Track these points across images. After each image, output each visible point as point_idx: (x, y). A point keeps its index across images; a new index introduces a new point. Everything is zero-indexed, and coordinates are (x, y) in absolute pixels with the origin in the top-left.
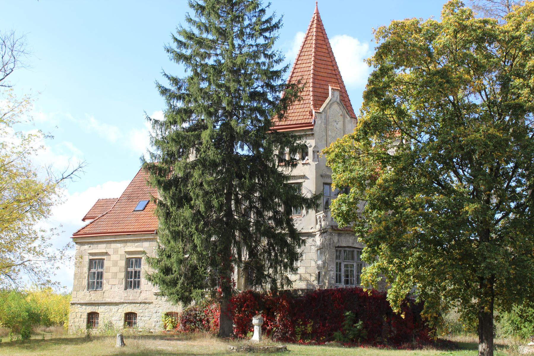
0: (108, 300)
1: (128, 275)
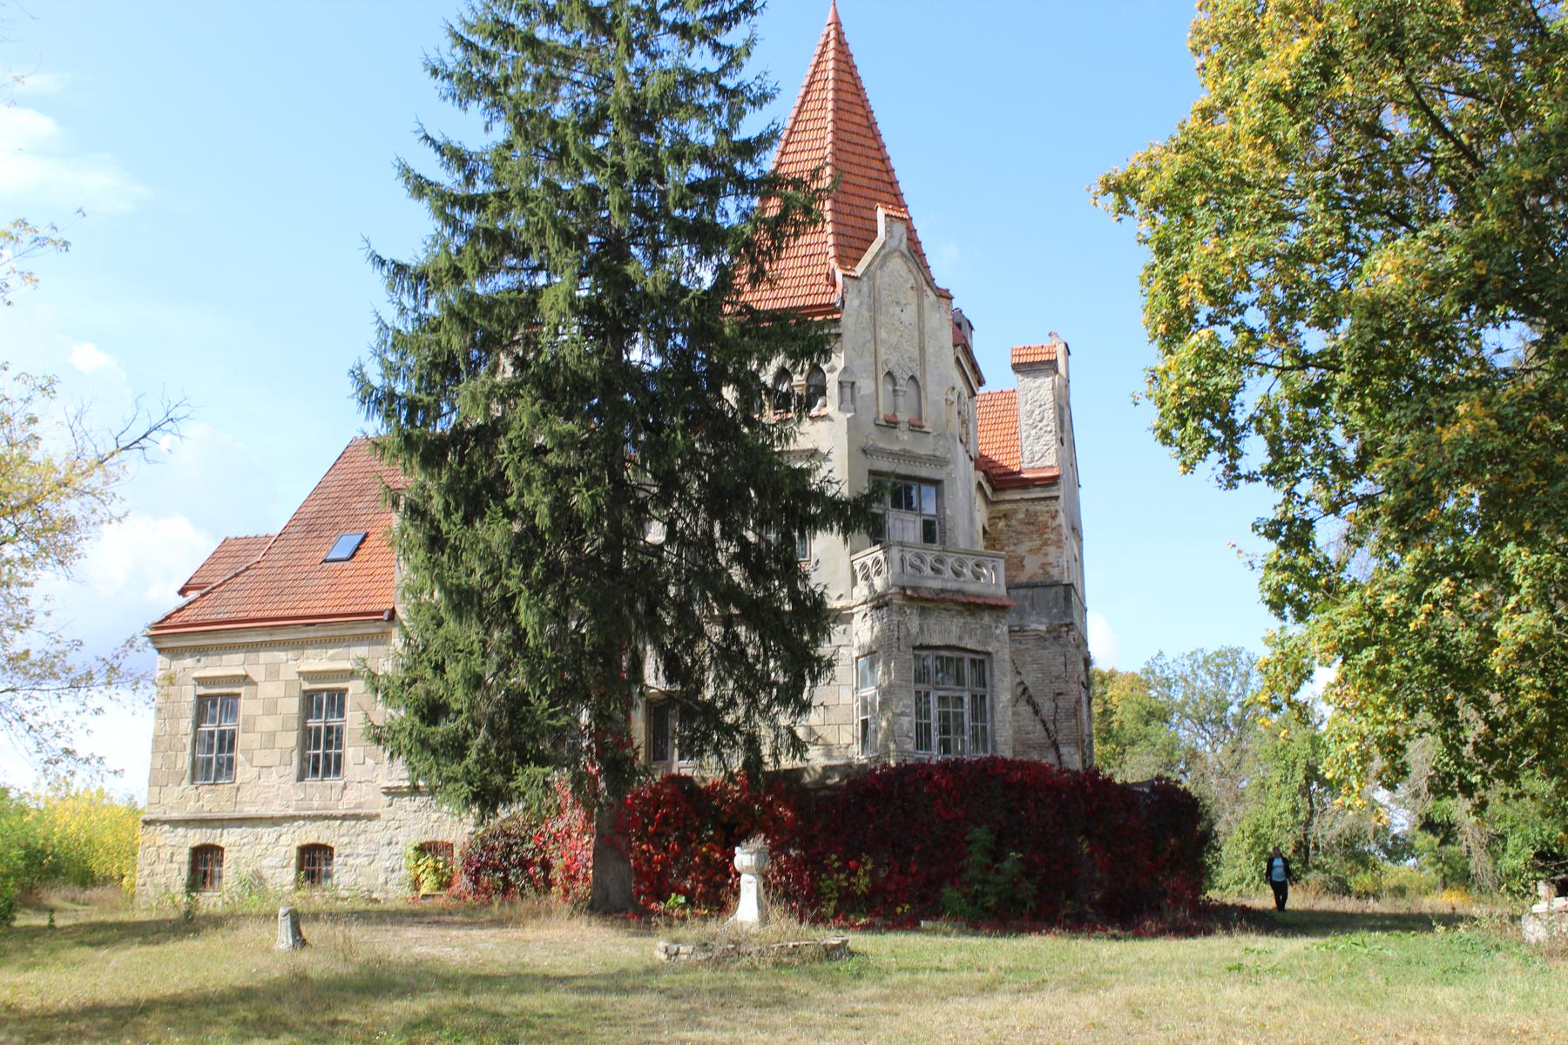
0: (250, 811)
1: (308, 738)
